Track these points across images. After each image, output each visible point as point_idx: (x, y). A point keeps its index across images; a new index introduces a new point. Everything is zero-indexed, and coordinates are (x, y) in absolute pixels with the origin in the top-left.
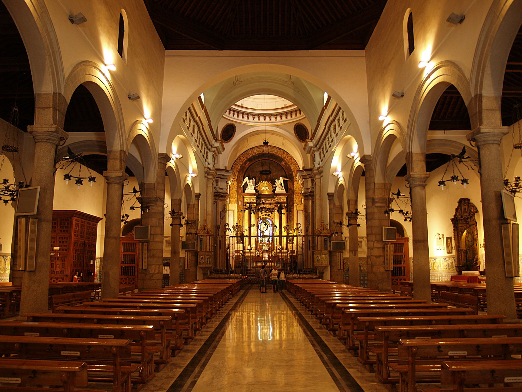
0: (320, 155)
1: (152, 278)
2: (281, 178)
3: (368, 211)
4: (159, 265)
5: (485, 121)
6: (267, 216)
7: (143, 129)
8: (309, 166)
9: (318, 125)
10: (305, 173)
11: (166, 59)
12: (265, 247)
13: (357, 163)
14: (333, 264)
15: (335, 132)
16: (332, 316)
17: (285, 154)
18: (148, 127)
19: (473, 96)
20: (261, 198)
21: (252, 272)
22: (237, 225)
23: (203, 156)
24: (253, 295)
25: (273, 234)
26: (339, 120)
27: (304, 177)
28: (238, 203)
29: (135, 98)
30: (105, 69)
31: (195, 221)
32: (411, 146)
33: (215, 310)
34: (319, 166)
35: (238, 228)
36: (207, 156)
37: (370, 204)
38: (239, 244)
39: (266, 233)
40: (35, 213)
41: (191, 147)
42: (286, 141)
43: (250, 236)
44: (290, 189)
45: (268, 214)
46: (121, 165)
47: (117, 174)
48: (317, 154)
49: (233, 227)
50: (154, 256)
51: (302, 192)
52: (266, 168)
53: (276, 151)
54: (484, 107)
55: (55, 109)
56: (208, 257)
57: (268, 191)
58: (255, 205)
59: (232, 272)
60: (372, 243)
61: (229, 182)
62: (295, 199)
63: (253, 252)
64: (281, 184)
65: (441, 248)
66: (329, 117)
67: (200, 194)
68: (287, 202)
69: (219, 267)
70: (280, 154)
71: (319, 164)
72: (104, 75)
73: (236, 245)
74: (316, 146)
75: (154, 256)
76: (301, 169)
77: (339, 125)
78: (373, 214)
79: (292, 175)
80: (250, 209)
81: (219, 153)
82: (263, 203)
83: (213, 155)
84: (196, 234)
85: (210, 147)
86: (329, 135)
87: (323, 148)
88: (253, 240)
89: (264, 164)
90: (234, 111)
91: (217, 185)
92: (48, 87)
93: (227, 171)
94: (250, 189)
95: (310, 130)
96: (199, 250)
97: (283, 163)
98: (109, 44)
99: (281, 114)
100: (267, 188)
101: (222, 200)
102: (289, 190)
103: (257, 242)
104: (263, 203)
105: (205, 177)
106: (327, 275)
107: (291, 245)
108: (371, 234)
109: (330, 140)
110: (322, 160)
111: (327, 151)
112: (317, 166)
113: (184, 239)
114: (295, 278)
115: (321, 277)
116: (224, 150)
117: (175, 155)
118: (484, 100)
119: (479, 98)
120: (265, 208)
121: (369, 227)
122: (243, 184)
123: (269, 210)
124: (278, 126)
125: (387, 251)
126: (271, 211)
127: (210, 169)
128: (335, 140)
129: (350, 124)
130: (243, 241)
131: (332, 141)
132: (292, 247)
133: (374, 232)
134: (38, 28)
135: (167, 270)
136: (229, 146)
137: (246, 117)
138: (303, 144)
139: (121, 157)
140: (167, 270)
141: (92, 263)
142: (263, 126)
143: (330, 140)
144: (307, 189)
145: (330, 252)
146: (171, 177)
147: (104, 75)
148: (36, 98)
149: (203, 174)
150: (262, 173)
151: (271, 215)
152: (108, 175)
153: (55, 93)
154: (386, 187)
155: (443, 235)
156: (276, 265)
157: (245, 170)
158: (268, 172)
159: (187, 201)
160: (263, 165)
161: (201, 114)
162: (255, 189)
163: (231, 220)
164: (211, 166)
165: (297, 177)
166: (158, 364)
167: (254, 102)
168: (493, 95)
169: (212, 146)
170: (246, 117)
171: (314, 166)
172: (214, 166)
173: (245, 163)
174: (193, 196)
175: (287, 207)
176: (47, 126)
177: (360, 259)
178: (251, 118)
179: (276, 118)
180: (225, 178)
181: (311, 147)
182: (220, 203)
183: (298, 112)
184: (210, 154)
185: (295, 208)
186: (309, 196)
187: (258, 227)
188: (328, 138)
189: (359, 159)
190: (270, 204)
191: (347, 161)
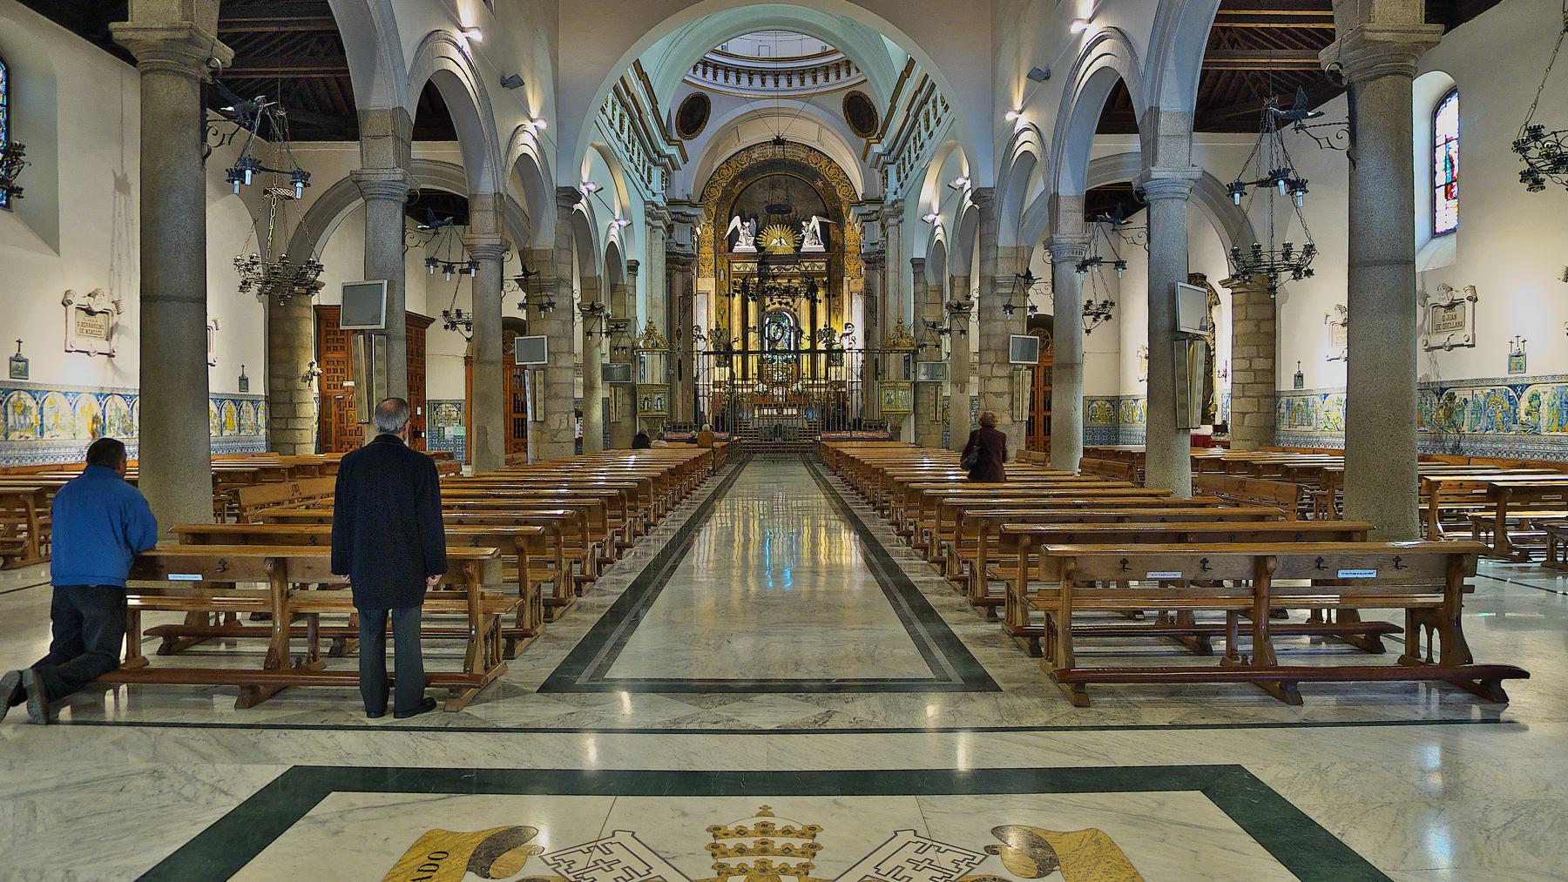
7: (526, 144)
8: (878, 193)
10: (868, 208)
14: (921, 411)
15: (927, 128)
16: (958, 540)
17: (824, 163)
23: (611, 124)
24: (752, 476)
25: (796, 344)
26: (935, 102)
27: (866, 219)
28: (717, 275)
29: (512, 83)
32: (1056, 185)
37: (988, 289)
43: (745, 353)
47: (491, 242)
48: (892, 170)
50: (557, 396)
52: (779, 197)
54: (1162, 132)
63: (752, 386)
68: (828, 273)
70: (812, 161)
72: (460, 50)
75: (557, 396)
79: (839, 210)
80: (744, 289)
82: (774, 277)
88: (753, 361)
92: (385, 95)
93: (694, 206)
103: (761, 362)
106: (908, 434)
112: (891, 198)
113: (607, 361)
114: (836, 440)
115: (895, 436)
116: (685, 160)
118: (1162, 118)
119: (1155, 112)
123: (787, 291)
126: (791, 292)
128: (927, 143)
136: (697, 146)
147: (460, 50)
148: (361, 119)
150: (771, 209)
160: (773, 187)
162: (755, 243)
163: (704, 317)
164: (659, 200)
166: (512, 638)
173: (733, 183)
181: (880, 155)
182: (678, 278)
184: (656, 173)
187: (762, 333)
191: (949, 193)
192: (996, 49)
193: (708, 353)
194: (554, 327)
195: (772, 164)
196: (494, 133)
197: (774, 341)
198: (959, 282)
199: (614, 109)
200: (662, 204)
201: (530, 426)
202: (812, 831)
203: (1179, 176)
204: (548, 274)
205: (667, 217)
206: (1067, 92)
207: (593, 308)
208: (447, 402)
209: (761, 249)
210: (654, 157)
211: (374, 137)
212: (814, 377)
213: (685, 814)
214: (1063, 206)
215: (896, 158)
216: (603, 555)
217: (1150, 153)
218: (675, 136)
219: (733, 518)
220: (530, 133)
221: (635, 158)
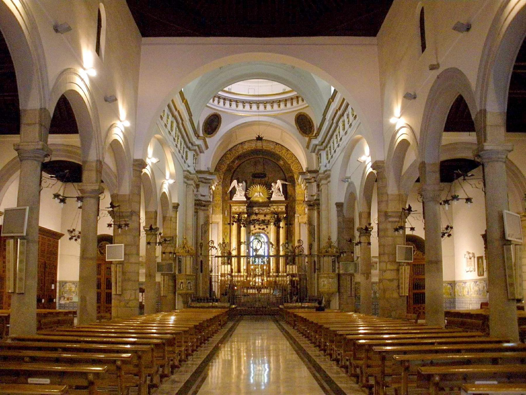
0: (327, 155)
1: (127, 305)
2: (279, 181)
3: (381, 227)
4: (135, 290)
5: (489, 138)
6: (261, 230)
8: (315, 168)
9: (324, 120)
10: (309, 176)
11: (142, 47)
13: (369, 170)
14: (342, 290)
15: (344, 129)
17: (284, 151)
18: (123, 130)
19: (478, 110)
20: (253, 207)
21: (242, 301)
22: (224, 243)
23: (182, 157)
24: (243, 328)
26: (348, 115)
27: (308, 181)
28: (223, 213)
30: (84, 74)
31: (173, 237)
33: (201, 340)
34: (325, 169)
35: (225, 245)
36: (187, 156)
37: (383, 219)
38: (223, 266)
39: (261, 252)
40: (25, 234)
41: (169, 146)
43: (239, 256)
45: (262, 227)
46: (97, 177)
47: (93, 188)
48: (323, 154)
49: (219, 245)
50: (129, 280)
51: (306, 200)
52: (259, 169)
53: (272, 147)
54: (488, 123)
55: (41, 125)
56: (189, 281)
57: (262, 198)
58: (246, 216)
59: (214, 300)
60: (385, 264)
61: (213, 188)
64: (279, 189)
65: (471, 269)
66: (337, 111)
67: (178, 205)
69: (201, 294)
71: (326, 166)
72: (82, 80)
73: (220, 267)
74: (322, 144)
75: (129, 280)
76: (305, 171)
77: (349, 121)
78: (386, 230)
80: (239, 221)
81: (201, 152)
82: (256, 214)
84: (175, 253)
85: (190, 145)
86: (337, 132)
87: (330, 147)
88: (243, 261)
89: (255, 163)
90: (219, 98)
91: (197, 191)
92: (35, 102)
93: (211, 174)
95: (316, 123)
96: (177, 273)
97: (281, 162)
98: (88, 46)
100: (261, 194)
102: (288, 196)
104: (256, 214)
105: (185, 182)
106: (335, 303)
107: (291, 267)
108: (384, 254)
111: (335, 151)
114: (295, 307)
116: (207, 147)
117: (151, 160)
118: (488, 116)
119: (483, 112)
121: (381, 245)
122: (230, 189)
124: (275, 117)
125: (402, 273)
127: (190, 173)
129: (360, 123)
130: (231, 261)
131: (341, 139)
134: (28, 45)
135: (141, 297)
136: (214, 141)
137: (234, 104)
138: (307, 139)
139: (97, 168)
140: (141, 297)
141: (53, 288)
142: (256, 115)
143: (339, 139)
144: (312, 196)
145: (339, 275)
146: (144, 185)
147: (82, 80)
148: (22, 114)
149: (181, 179)
150: (255, 176)
151: (266, 228)
152: (83, 187)
153: (41, 109)
154: (402, 198)
155: (473, 254)
156: (272, 291)
157: (233, 170)
159: (163, 213)
160: (255, 164)
161: (181, 107)
162: (246, 195)
163: (216, 236)
164: (191, 169)
165: (299, 181)
167: (242, 89)
168: (498, 111)
169: (192, 144)
170: (234, 104)
171: (320, 168)
172: (195, 169)
173: (233, 162)
174: (171, 207)
176: (34, 144)
177: (374, 283)
178: (240, 106)
179: (272, 106)
180: (208, 182)
181: (316, 146)
182: (201, 214)
183: (300, 99)
184: (190, 154)
185: (296, 220)
186: (314, 205)
188: (337, 135)
192: (383, 86)
193: (218, 257)
195: (256, 152)
196: (98, 127)
197: (256, 250)
198: (365, 215)
199: (168, 118)
200: (193, 171)
201: (113, 296)
203: (500, 148)
204: (125, 209)
205: (196, 179)
207: (151, 228)
208: (70, 282)
210: (189, 145)
211: (29, 125)
212: (278, 271)
214: (428, 169)
215: (326, 146)
216: (163, 372)
217: (482, 138)
218: (201, 134)
219: (232, 356)
220: (120, 127)
221: (179, 145)
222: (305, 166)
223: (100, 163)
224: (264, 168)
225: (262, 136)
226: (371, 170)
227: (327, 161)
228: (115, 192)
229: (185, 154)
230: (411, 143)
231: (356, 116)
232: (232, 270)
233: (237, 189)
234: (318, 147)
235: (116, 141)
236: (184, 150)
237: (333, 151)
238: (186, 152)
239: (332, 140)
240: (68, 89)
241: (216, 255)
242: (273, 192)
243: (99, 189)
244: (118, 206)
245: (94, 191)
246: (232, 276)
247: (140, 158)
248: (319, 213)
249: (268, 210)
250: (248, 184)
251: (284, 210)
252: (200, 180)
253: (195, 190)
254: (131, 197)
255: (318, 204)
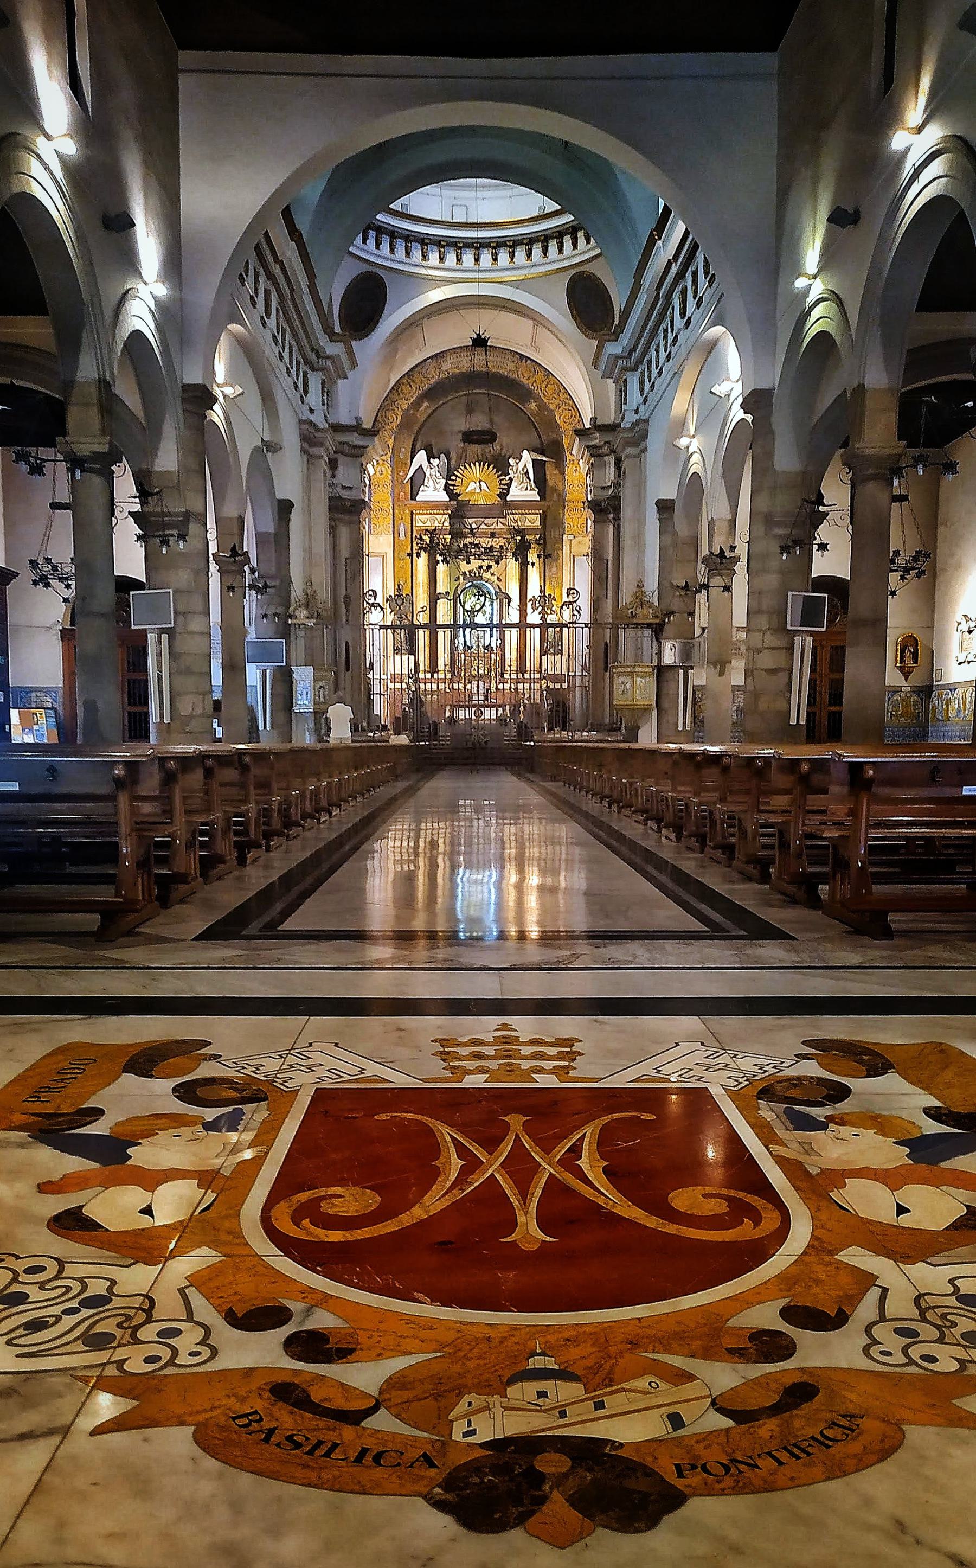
0: (642, 383)
8: (610, 417)
10: (597, 440)
12: (479, 668)
15: (683, 314)
18: (153, 308)
23: (296, 387)
26: (695, 274)
27: (595, 452)
35: (401, 600)
37: (760, 530)
38: (398, 657)
42: (542, 331)
44: (555, 490)
45: (486, 563)
52: (479, 422)
56: (321, 684)
61: (370, 467)
62: (567, 519)
64: (527, 473)
70: (524, 377)
72: (46, 167)
76: (588, 426)
77: (695, 292)
80: (431, 549)
81: (339, 377)
83: (323, 383)
87: (649, 362)
91: (333, 476)
94: (432, 491)
99: (529, 242)
100: (484, 486)
101: (350, 523)
107: (551, 658)
108: (759, 612)
109: (670, 338)
110: (646, 400)
112: (630, 418)
116: (354, 364)
120: (477, 546)
131: (675, 340)
132: (555, 664)
133: (764, 607)
136: (370, 348)
138: (595, 343)
143: (670, 338)
144: (603, 488)
147: (46, 167)
150: (469, 437)
158: (487, 437)
160: (470, 410)
162: (446, 488)
163: (378, 579)
164: (318, 419)
169: (318, 356)
175: (543, 542)
179: (512, 256)
181: (618, 357)
183: (580, 235)
184: (315, 381)
186: (606, 509)
187: (456, 599)
188: (666, 331)
189: (740, 400)
190: (493, 535)
194: (182, 577)
195: (470, 379)
200: (322, 424)
202: (569, 1042)
206: (883, 239)
209: (452, 495)
210: (312, 359)
213: (401, 1030)
215: (640, 362)
218: (337, 329)
221: (286, 355)
222: (587, 415)
223: (104, 385)
224: (491, 421)
225: (487, 335)
226: (741, 414)
227: (641, 399)
228: (144, 466)
229: (301, 379)
230: (838, 339)
231: (713, 275)
232: (417, 664)
233: (428, 474)
234: (620, 362)
235: (137, 335)
236: (298, 370)
237: (655, 372)
238: (305, 374)
239: (655, 342)
240: (16, 190)
241: (382, 623)
242: (511, 479)
243: (110, 453)
244: (158, 493)
245: (96, 456)
246: (417, 681)
247: (199, 381)
248: (618, 529)
249: (500, 526)
250: (453, 462)
251: (538, 523)
252: (340, 447)
253: (329, 473)
254: (182, 478)
255: (617, 509)
